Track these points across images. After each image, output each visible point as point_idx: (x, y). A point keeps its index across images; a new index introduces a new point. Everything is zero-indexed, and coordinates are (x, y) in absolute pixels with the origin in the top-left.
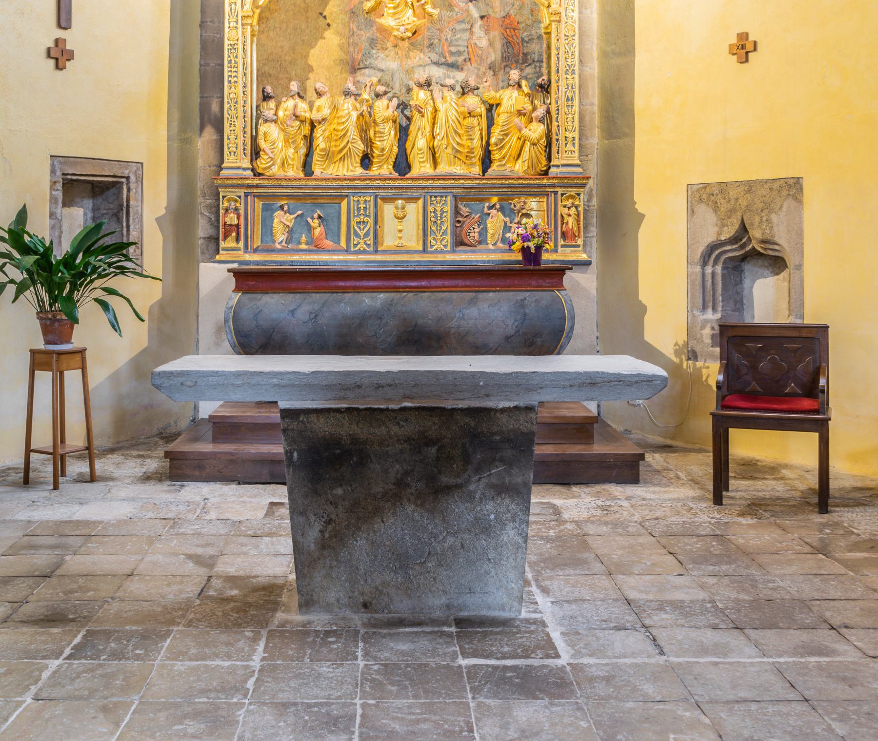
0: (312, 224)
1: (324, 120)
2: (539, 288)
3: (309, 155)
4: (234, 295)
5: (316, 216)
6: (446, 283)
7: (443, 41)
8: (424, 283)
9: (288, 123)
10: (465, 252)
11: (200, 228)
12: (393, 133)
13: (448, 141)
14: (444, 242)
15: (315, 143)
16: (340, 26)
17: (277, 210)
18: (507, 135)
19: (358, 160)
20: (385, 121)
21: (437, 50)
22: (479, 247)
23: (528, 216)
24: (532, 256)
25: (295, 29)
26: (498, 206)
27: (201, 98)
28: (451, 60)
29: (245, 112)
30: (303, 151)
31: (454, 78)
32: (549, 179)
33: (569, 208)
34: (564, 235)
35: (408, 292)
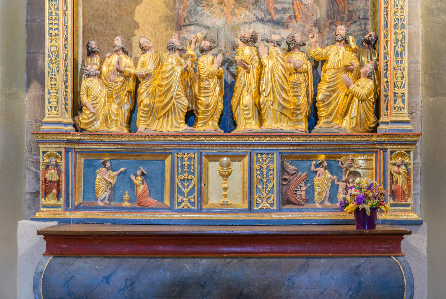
0: (135, 181)
1: (148, 75)
2: (374, 253)
3: (133, 111)
4: (44, 259)
5: (139, 173)
6: (274, 248)
8: (249, 249)
9: (112, 78)
10: (292, 211)
11: (27, 183)
12: (218, 89)
13: (274, 97)
14: (270, 201)
15: (140, 98)
17: (99, 167)
18: (334, 91)
19: (182, 116)
20: (210, 76)
21: (262, 7)
22: (307, 206)
23: (356, 174)
24: (365, 219)
26: (325, 164)
27: (28, 53)
28: (276, 17)
29: (66, 66)
30: (127, 107)
31: (279, 34)
32: (379, 136)
33: (399, 166)
34: (393, 194)
35: (233, 257)
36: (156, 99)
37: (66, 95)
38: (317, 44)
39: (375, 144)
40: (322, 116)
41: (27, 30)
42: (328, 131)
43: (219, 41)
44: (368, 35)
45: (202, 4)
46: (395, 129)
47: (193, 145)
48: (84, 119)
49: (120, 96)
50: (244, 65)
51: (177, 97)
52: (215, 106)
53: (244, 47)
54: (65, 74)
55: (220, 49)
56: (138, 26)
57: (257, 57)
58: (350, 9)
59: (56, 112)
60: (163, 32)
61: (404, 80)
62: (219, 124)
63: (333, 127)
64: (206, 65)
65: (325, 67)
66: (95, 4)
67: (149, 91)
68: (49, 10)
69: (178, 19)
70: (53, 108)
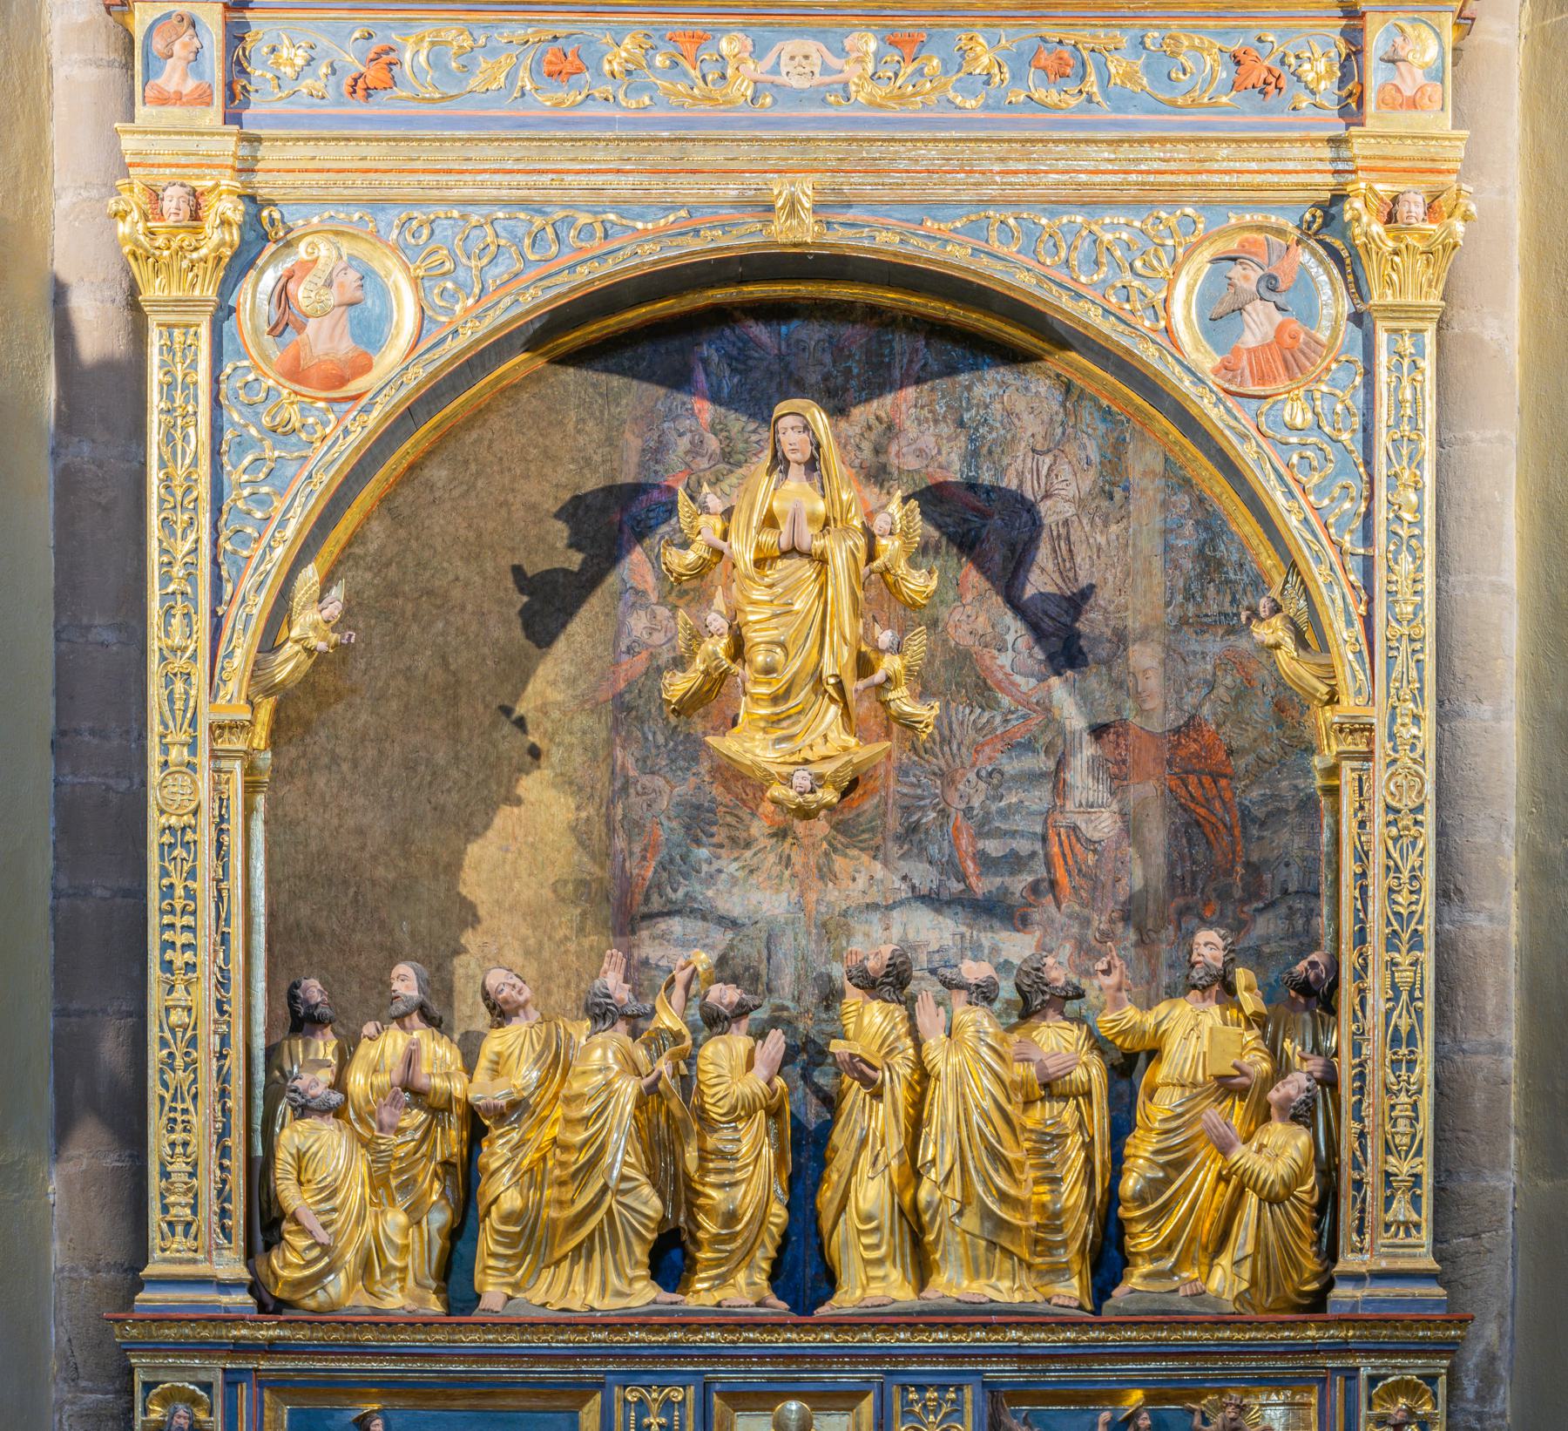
3: (461, 1232)
7: (956, 816)
9: (386, 1116)
12: (768, 1153)
16: (578, 758)
18: (1179, 1165)
19: (641, 1253)
20: (742, 1111)
21: (933, 850)
25: (410, 766)
27: (61, 1013)
28: (983, 886)
30: (439, 1218)
32: (1326, 1325)
36: (547, 1193)
37: (224, 1182)
38: (1124, 994)
39: (1318, 1352)
40: (1138, 1254)
41: (56, 926)
42: (1156, 1306)
43: (773, 975)
44: (1304, 963)
45: (712, 835)
46: (1384, 1301)
47: (679, 1356)
48: (287, 1265)
49: (414, 1180)
50: (862, 1072)
51: (623, 1186)
52: (759, 1215)
53: (865, 1002)
54: (218, 1107)
55: (778, 1002)
56: (475, 915)
57: (909, 1042)
58: (1254, 858)
59: (191, 1243)
60: (566, 938)
61: (1419, 1126)
62: (772, 1278)
63: (1176, 1291)
64: (725, 1072)
65: (1154, 1075)
66: (314, 832)
67: (520, 1163)
68: (161, 878)
69: (624, 893)
70: (179, 1229)
